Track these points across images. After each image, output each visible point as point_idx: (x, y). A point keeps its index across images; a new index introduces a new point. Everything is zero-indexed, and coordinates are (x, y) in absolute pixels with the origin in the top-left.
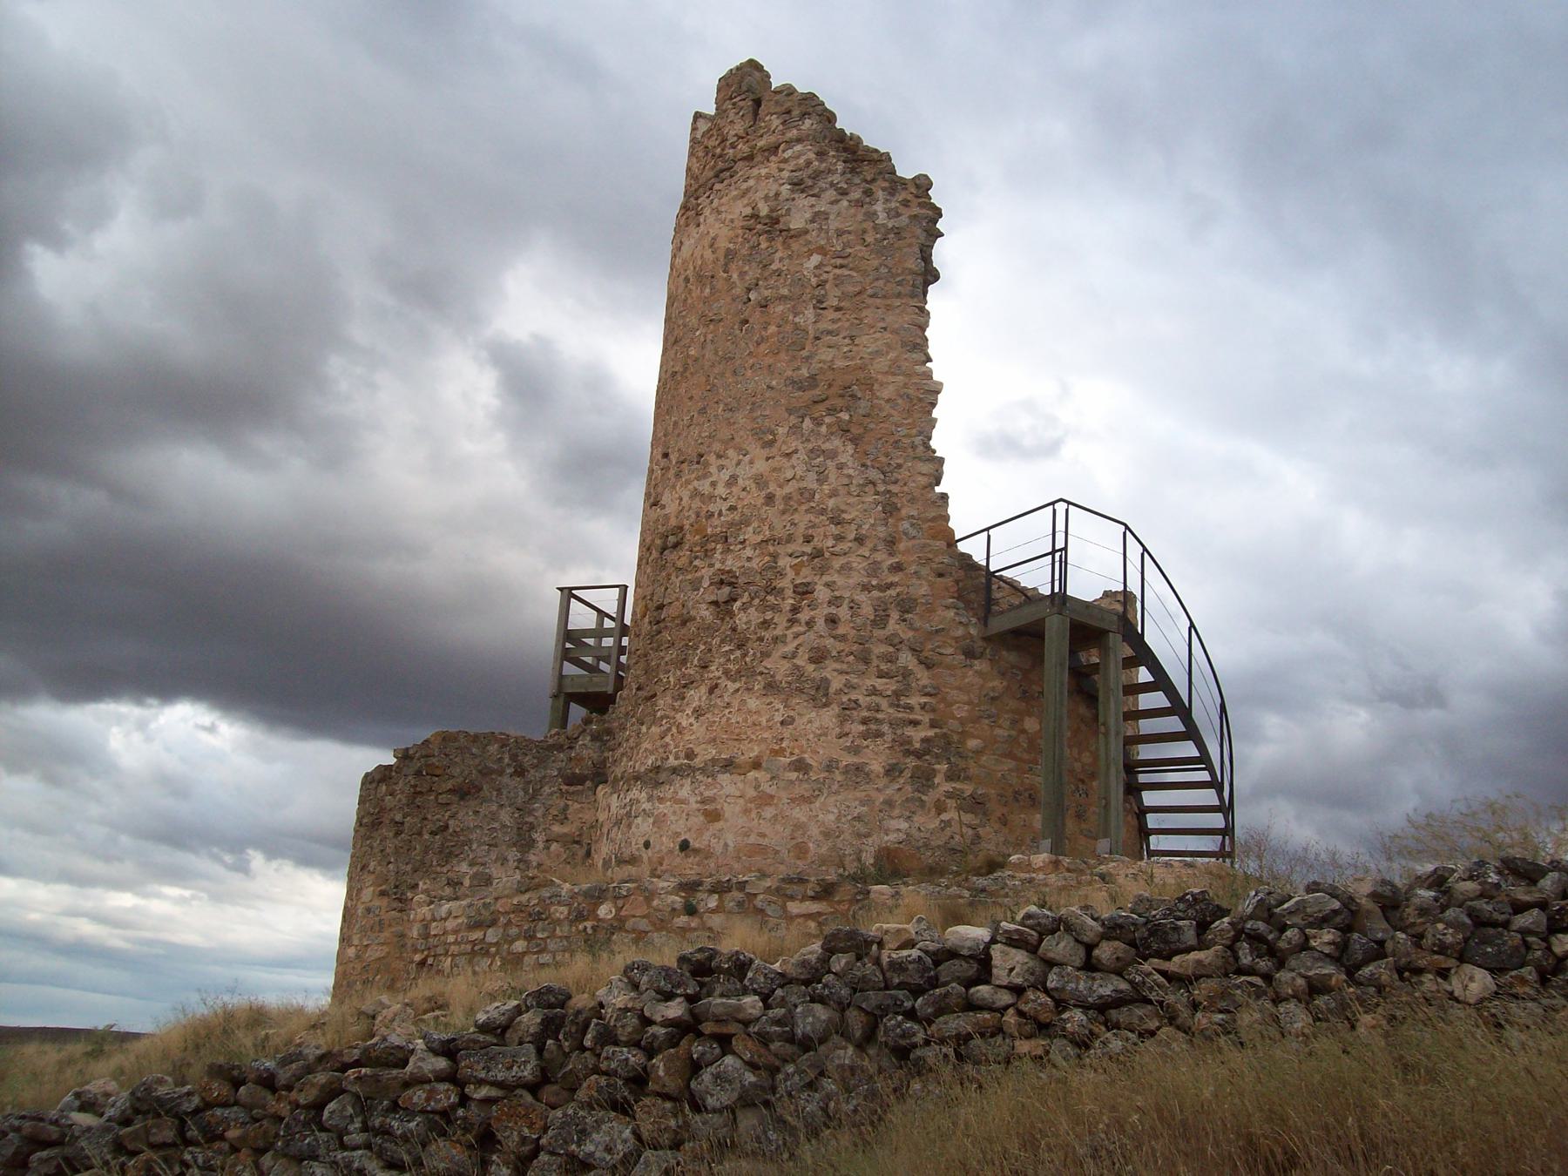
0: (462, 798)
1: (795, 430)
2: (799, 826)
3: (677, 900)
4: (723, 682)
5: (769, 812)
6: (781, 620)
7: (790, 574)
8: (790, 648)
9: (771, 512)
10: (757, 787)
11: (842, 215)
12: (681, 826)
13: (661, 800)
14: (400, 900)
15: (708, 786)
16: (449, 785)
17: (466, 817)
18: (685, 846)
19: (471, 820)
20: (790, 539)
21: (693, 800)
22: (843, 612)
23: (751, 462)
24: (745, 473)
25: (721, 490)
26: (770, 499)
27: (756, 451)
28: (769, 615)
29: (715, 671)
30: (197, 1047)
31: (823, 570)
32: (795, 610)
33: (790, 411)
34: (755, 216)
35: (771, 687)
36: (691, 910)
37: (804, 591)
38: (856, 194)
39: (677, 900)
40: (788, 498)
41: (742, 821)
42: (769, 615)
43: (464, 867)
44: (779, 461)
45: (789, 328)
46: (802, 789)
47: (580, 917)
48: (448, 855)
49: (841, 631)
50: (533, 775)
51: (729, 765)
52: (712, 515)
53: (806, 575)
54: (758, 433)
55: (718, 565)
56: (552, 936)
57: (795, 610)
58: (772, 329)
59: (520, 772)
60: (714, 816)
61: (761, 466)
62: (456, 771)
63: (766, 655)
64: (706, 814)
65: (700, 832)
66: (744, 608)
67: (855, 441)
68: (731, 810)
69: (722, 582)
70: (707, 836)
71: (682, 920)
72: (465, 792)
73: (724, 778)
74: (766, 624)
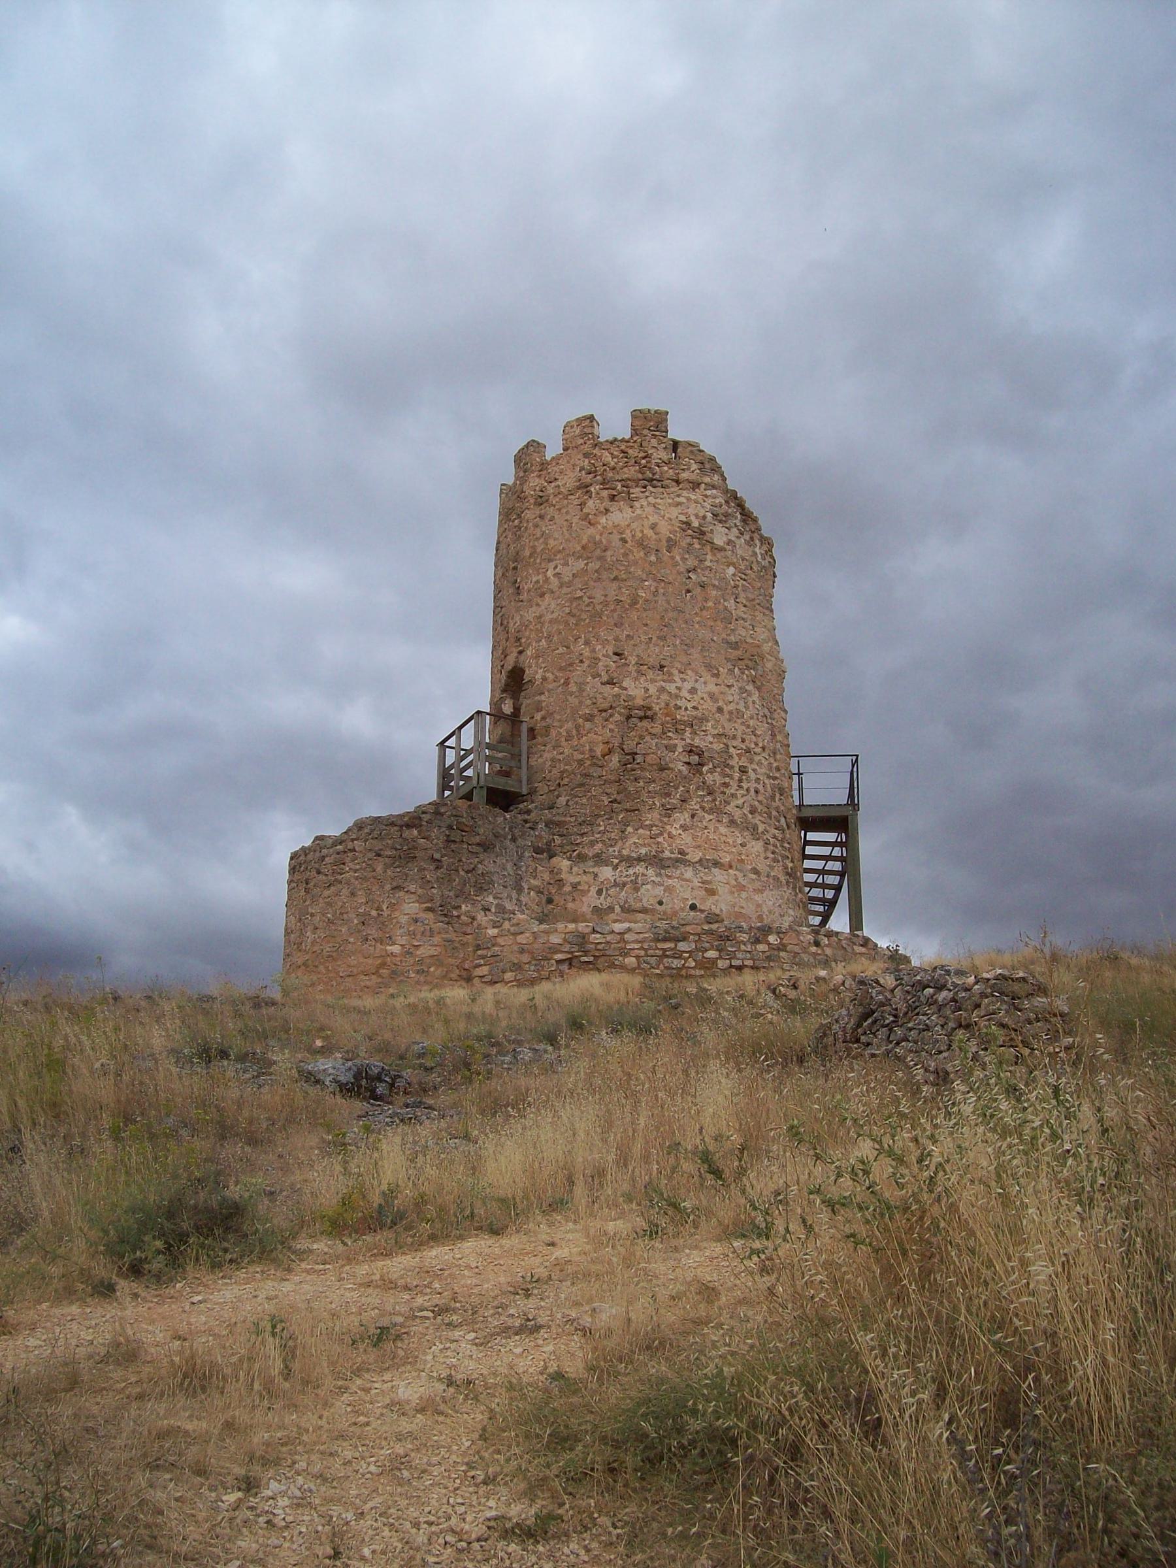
0: (485, 851)
1: (731, 671)
2: (759, 906)
3: (810, 938)
4: (700, 813)
5: (744, 895)
6: (734, 784)
7: (736, 759)
8: (740, 802)
9: (723, 719)
10: (736, 880)
11: (742, 550)
12: (690, 897)
13: (669, 877)
14: (445, 915)
15: (706, 874)
16: (477, 839)
17: (488, 864)
18: (693, 907)
19: (492, 868)
20: (734, 737)
21: (696, 881)
22: (760, 787)
23: (705, 683)
24: (702, 690)
25: (684, 693)
26: (720, 710)
27: (707, 677)
28: (727, 780)
29: (694, 804)
30: (1089, 968)
31: (751, 761)
32: (740, 781)
33: (728, 660)
34: (688, 524)
35: (732, 822)
36: (817, 944)
37: (743, 770)
38: (747, 537)
39: (810, 938)
40: (730, 713)
41: (730, 898)
42: (727, 780)
43: (491, 899)
44: (723, 688)
45: (721, 607)
46: (758, 885)
47: (757, 941)
48: (481, 890)
49: (760, 798)
50: (520, 841)
51: (716, 864)
52: (680, 708)
53: (744, 762)
54: (709, 667)
55: (688, 741)
56: (739, 950)
57: (740, 781)
58: (710, 604)
59: (514, 840)
60: (712, 892)
61: (711, 687)
62: (481, 831)
63: (727, 803)
64: (707, 890)
65: (703, 900)
66: (711, 771)
67: (758, 688)
68: (722, 890)
69: (691, 751)
70: (708, 903)
71: (814, 949)
72: (486, 847)
73: (716, 871)
74: (726, 785)
